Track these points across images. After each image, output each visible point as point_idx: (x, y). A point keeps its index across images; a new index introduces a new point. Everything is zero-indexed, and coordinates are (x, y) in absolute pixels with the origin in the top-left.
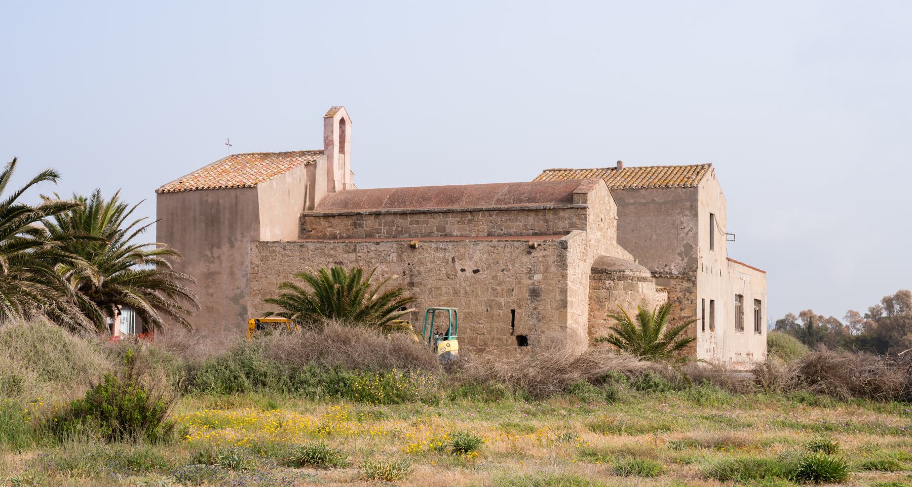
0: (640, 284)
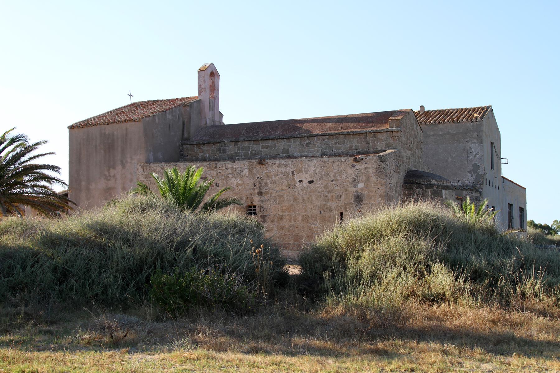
0: (443, 191)
